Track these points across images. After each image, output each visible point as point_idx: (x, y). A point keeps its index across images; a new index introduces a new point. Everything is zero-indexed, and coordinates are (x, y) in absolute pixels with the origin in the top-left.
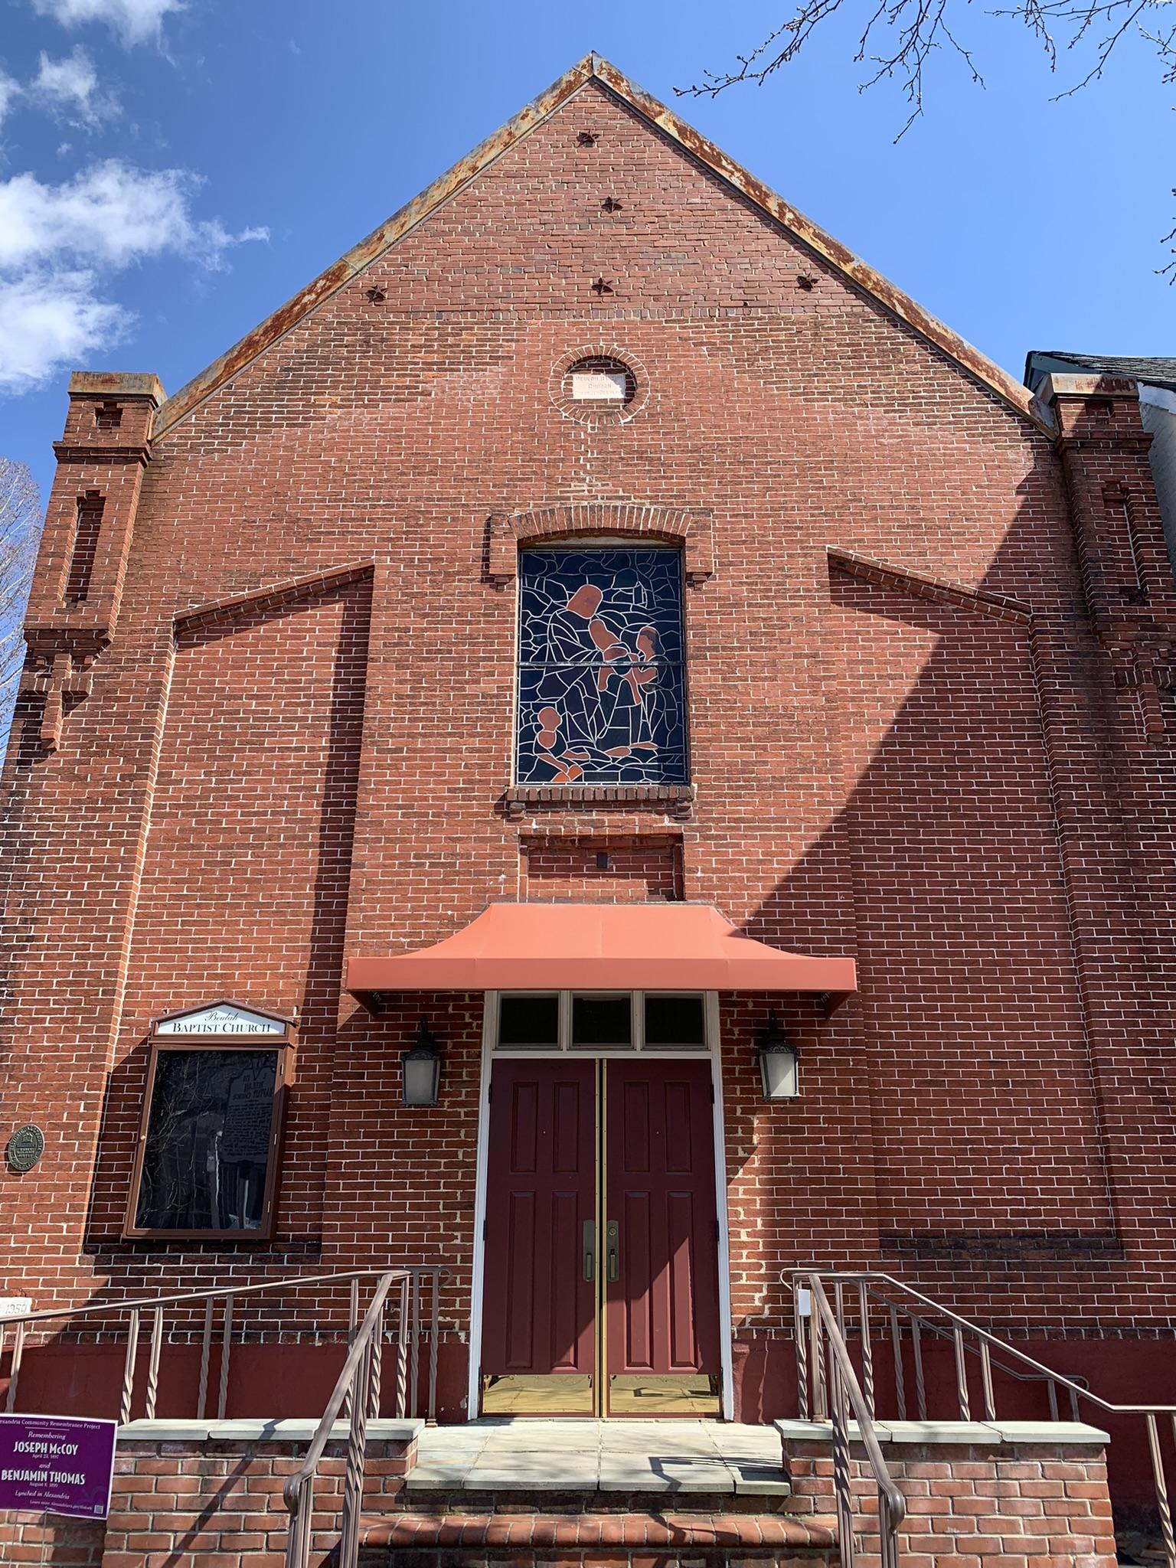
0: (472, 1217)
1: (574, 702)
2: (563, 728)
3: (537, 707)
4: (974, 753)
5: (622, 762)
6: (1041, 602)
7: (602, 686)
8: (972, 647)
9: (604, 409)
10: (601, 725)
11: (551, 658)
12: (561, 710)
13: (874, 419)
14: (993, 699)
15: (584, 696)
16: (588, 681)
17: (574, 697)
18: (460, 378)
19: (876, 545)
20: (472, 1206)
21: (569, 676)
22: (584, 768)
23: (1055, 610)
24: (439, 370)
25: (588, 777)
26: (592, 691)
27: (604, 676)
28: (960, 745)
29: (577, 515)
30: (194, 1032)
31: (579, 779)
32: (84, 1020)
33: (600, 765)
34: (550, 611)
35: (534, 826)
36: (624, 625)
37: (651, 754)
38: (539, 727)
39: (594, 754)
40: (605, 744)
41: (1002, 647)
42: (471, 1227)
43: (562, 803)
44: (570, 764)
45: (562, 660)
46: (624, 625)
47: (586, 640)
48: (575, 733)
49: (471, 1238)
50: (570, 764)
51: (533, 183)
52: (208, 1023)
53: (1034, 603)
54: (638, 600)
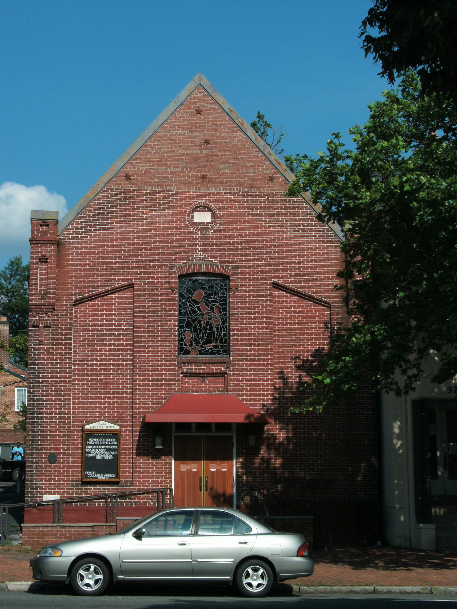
0: (171, 475)
1: (195, 330)
2: (192, 338)
3: (184, 331)
4: (311, 348)
5: (210, 349)
6: (334, 301)
7: (204, 324)
8: (313, 313)
9: (204, 227)
10: (203, 337)
11: (188, 315)
12: (191, 332)
13: (289, 233)
14: (317, 330)
15: (198, 327)
16: (199, 322)
17: (195, 328)
18: (157, 213)
19: (287, 280)
20: (171, 473)
21: (194, 321)
22: (199, 351)
23: (338, 303)
24: (150, 210)
25: (200, 354)
26: (201, 326)
27: (204, 320)
28: (307, 345)
29: (196, 267)
30: (95, 428)
31: (197, 354)
32: (63, 424)
33: (203, 350)
34: (188, 299)
35: (185, 370)
36: (210, 304)
37: (218, 347)
38: (185, 338)
39: (202, 347)
40: (204, 343)
41: (321, 314)
42: (171, 478)
43: (131, 495)
44: (194, 349)
45: (191, 315)
46: (210, 304)
47: (198, 308)
48: (196, 340)
49: (171, 481)
50: (194, 349)
51: (180, 132)
52: (98, 426)
53: (332, 301)
54: (215, 295)
